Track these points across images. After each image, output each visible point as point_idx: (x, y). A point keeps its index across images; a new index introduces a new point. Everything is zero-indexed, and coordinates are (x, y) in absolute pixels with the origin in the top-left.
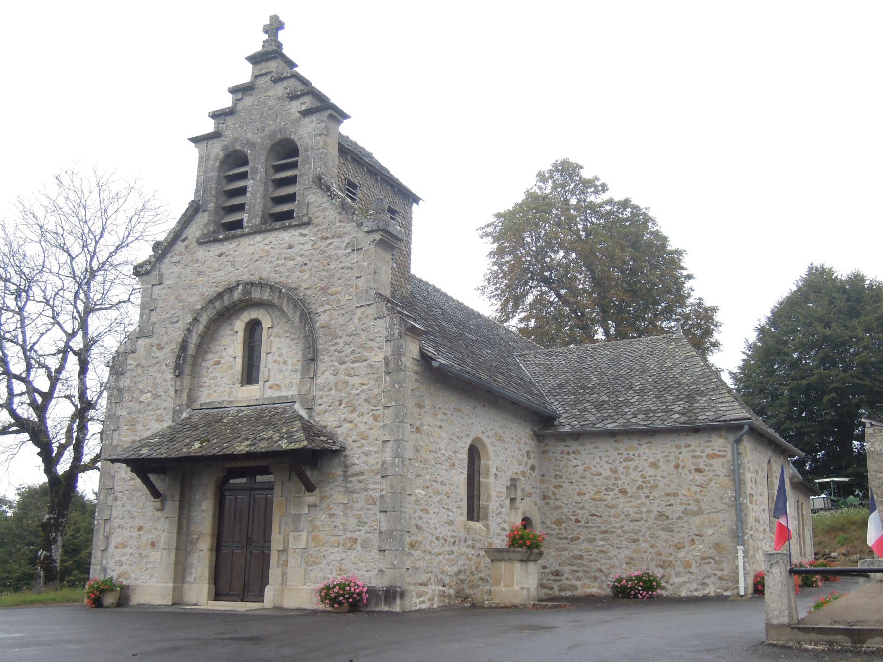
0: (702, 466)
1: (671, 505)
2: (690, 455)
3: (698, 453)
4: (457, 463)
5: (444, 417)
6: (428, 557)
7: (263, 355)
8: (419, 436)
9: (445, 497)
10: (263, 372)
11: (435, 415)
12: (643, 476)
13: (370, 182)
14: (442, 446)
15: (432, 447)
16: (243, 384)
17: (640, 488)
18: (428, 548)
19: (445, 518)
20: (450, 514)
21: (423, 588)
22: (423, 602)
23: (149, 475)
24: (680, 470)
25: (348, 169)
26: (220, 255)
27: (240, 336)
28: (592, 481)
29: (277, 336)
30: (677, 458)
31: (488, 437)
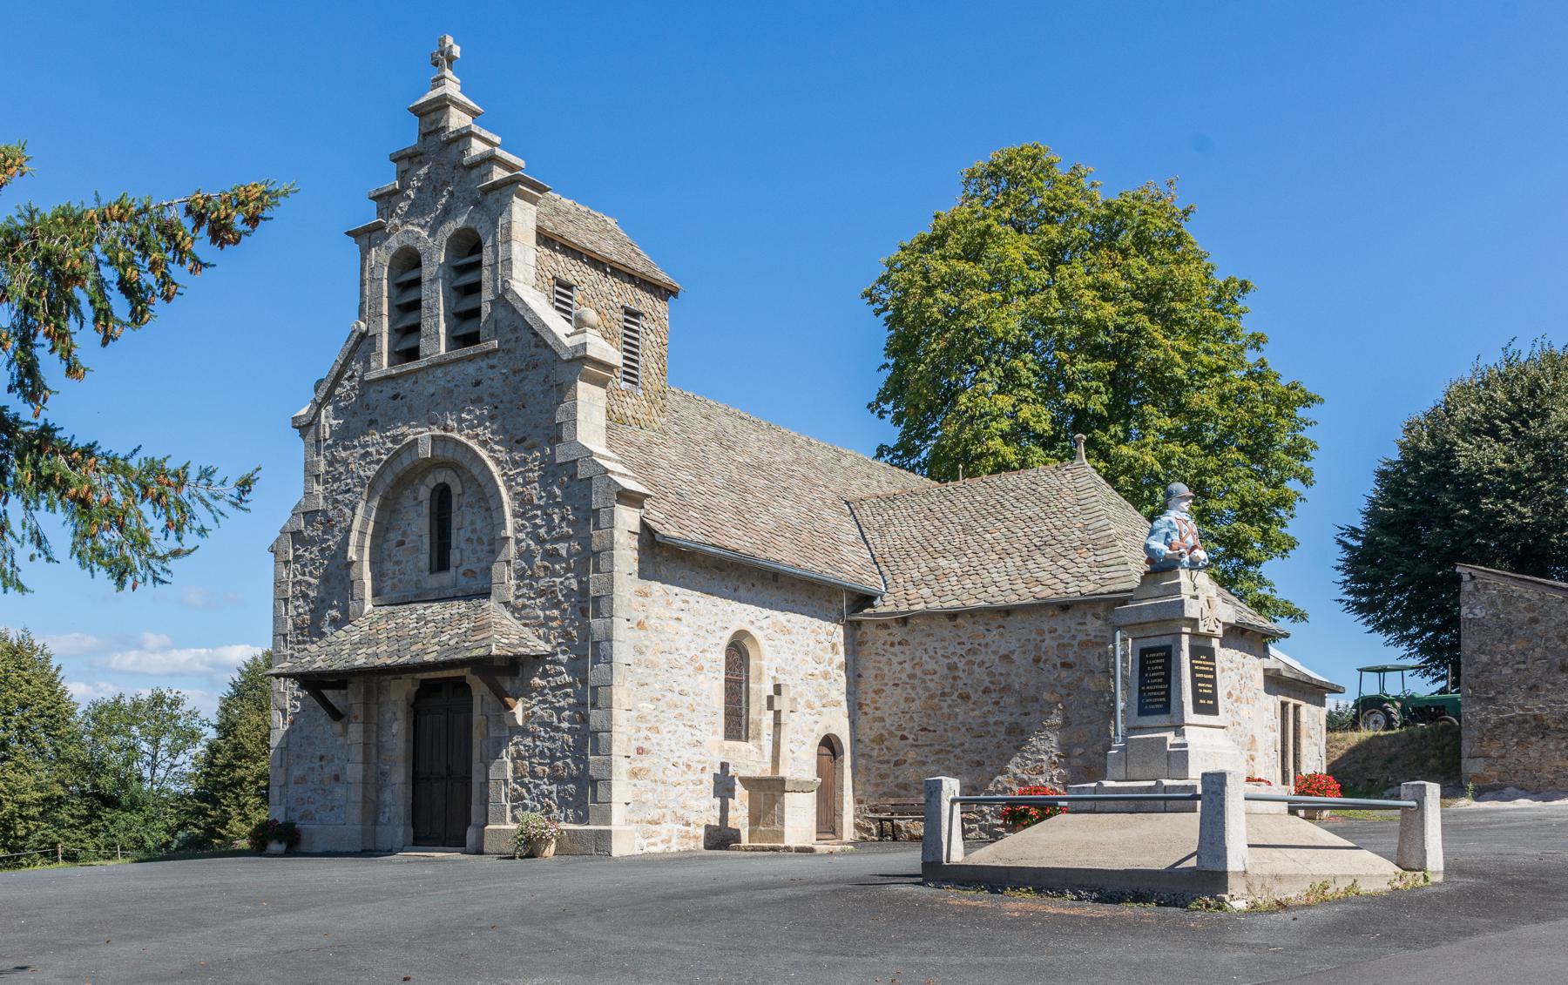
0: (1071, 659)
1: (1026, 714)
2: (1054, 644)
3: (1066, 641)
4: (706, 666)
5: (684, 606)
6: (660, 787)
7: (454, 532)
8: (642, 633)
9: (685, 711)
10: (455, 556)
11: (669, 604)
12: (991, 674)
13: (594, 275)
14: (681, 643)
15: (666, 646)
16: (432, 572)
17: (986, 691)
18: (660, 776)
19: (688, 738)
20: (696, 732)
21: (653, 827)
22: (654, 844)
23: (325, 692)
24: (1041, 665)
25: (557, 263)
26: (395, 397)
27: (425, 509)
28: (924, 681)
29: (470, 505)
30: (1038, 648)
31: (761, 628)
